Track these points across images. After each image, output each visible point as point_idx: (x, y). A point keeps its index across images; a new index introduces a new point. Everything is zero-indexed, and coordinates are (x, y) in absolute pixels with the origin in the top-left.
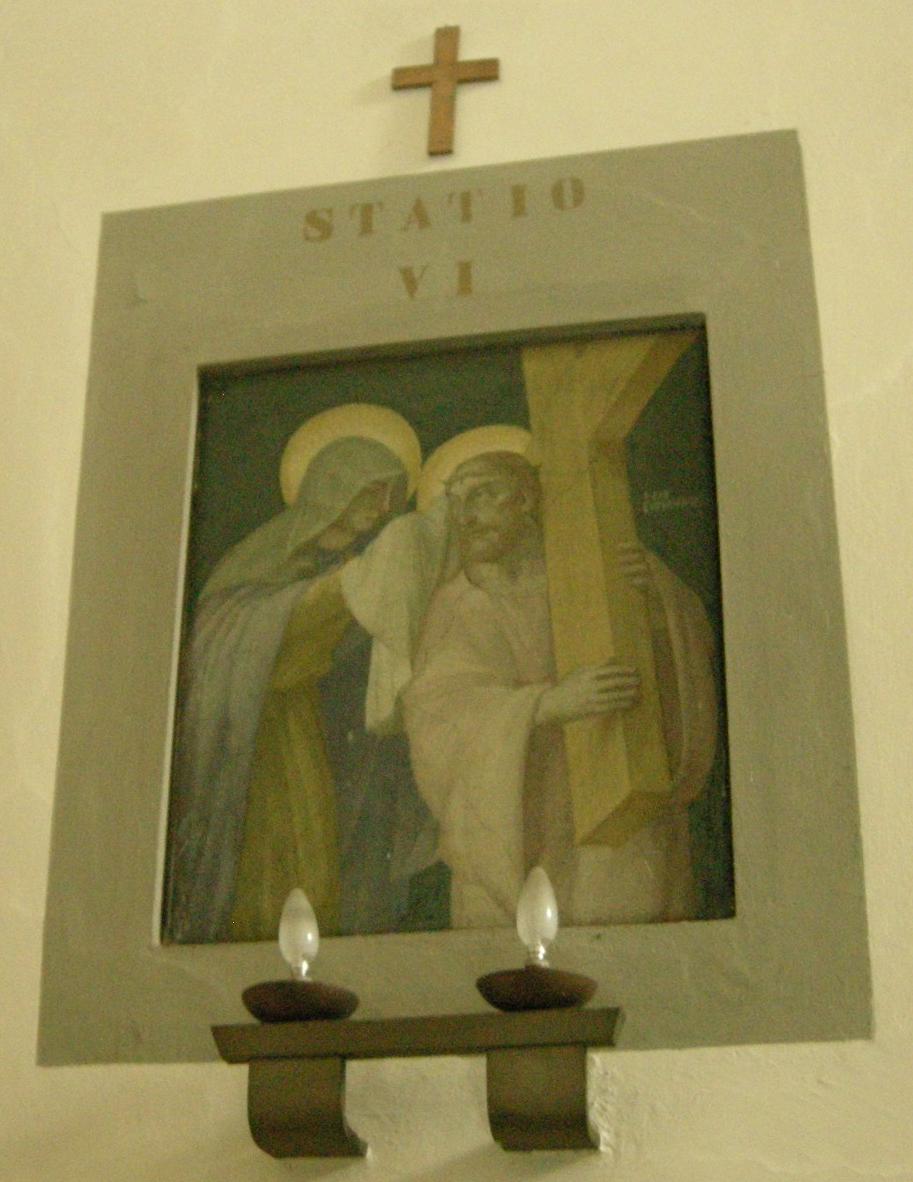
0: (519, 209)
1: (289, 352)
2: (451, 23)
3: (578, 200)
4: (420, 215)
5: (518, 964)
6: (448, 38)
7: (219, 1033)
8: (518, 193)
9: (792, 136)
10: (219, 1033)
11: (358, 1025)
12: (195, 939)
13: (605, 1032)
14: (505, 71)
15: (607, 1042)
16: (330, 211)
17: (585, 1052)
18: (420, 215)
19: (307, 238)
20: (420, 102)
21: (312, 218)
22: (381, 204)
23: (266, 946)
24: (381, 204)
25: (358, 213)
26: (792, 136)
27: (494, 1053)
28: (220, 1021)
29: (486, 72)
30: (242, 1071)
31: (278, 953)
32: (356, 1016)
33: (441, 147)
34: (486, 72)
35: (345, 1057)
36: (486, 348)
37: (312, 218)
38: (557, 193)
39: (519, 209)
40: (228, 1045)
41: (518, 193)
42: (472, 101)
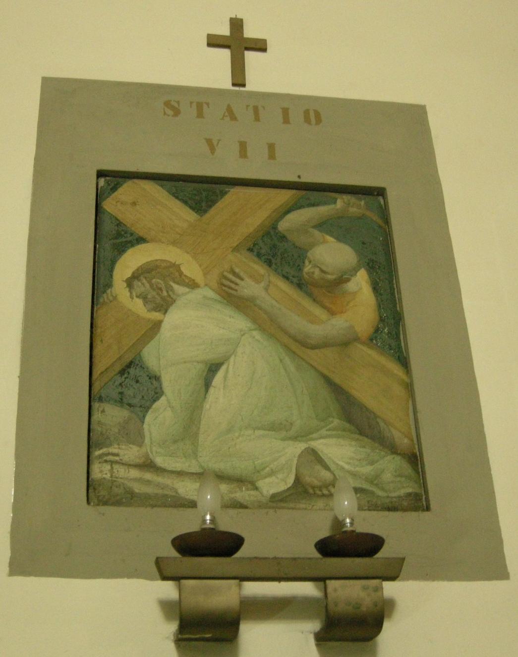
3: (319, 120)
6: (237, 24)
8: (285, 112)
10: (158, 562)
29: (260, 46)
33: (239, 79)
34: (260, 46)
38: (307, 112)
41: (285, 112)
42: (250, 57)
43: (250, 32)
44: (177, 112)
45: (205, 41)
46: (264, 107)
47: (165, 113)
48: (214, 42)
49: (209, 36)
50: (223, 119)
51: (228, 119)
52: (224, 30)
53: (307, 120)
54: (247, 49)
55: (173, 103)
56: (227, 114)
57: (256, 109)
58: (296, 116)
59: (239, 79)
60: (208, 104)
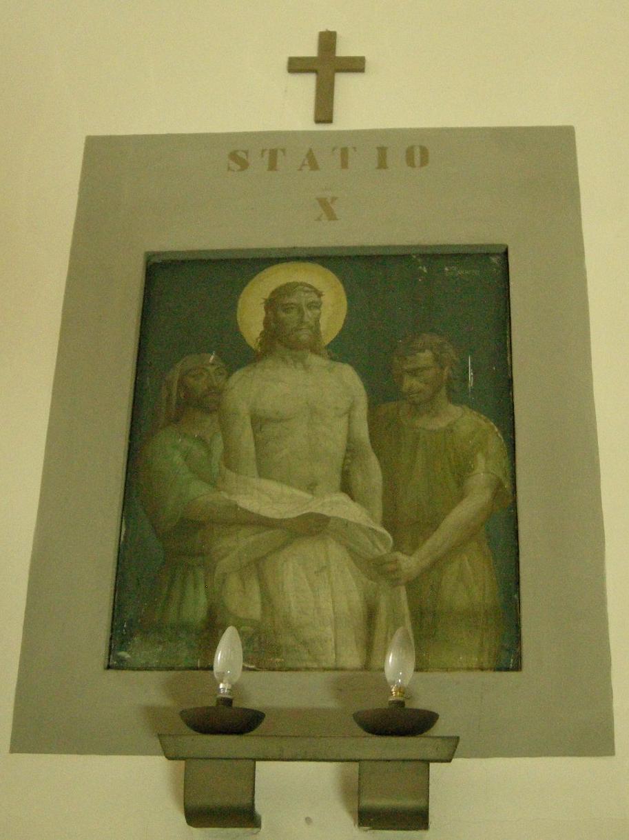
0: (382, 164)
2: (331, 29)
4: (312, 162)
5: (211, 702)
6: (328, 40)
8: (382, 151)
9: (567, 134)
12: (519, 657)
13: (450, 750)
14: (367, 66)
16: (246, 152)
18: (312, 162)
19: (229, 169)
20: (308, 83)
22: (283, 150)
25: (267, 155)
26: (567, 134)
29: (356, 65)
31: (213, 675)
33: (324, 112)
34: (356, 65)
35: (254, 760)
37: (234, 156)
39: (382, 164)
41: (382, 151)
42: (345, 83)
44: (244, 165)
46: (355, 148)
47: (246, 152)
48: (297, 66)
51: (307, 169)
52: (310, 50)
55: (239, 154)
56: (306, 162)
57: (344, 151)
58: (396, 160)
59: (324, 112)
60: (283, 150)
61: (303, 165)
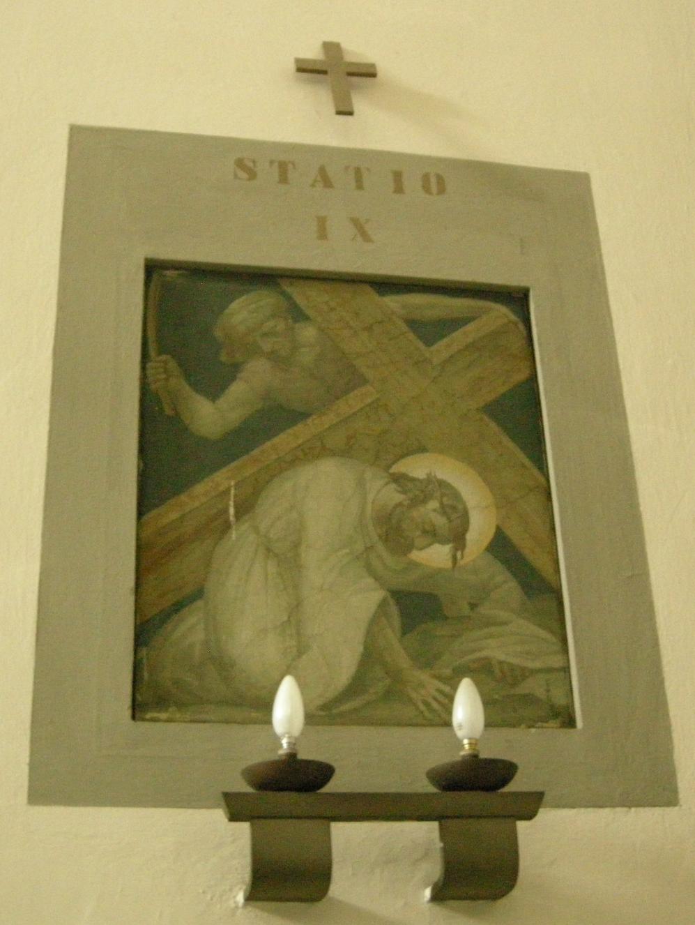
1: (201, 261)
3: (442, 190)
7: (227, 796)
8: (398, 176)
11: (320, 794)
13: (529, 805)
15: (530, 816)
17: (515, 823)
21: (240, 163)
23: (266, 727)
24: (368, 169)
25: (276, 164)
27: (256, 821)
28: (227, 790)
30: (244, 828)
32: (511, 787)
36: (210, 271)
37: (240, 163)
38: (426, 178)
40: (237, 809)
41: (398, 176)
43: (358, 49)
44: (252, 175)
45: (292, 66)
47: (254, 162)
49: (298, 61)
50: (313, 186)
52: (313, 52)
53: (426, 188)
54: (350, 74)
56: (319, 179)
57: (358, 171)
58: (412, 183)
61: (315, 181)
